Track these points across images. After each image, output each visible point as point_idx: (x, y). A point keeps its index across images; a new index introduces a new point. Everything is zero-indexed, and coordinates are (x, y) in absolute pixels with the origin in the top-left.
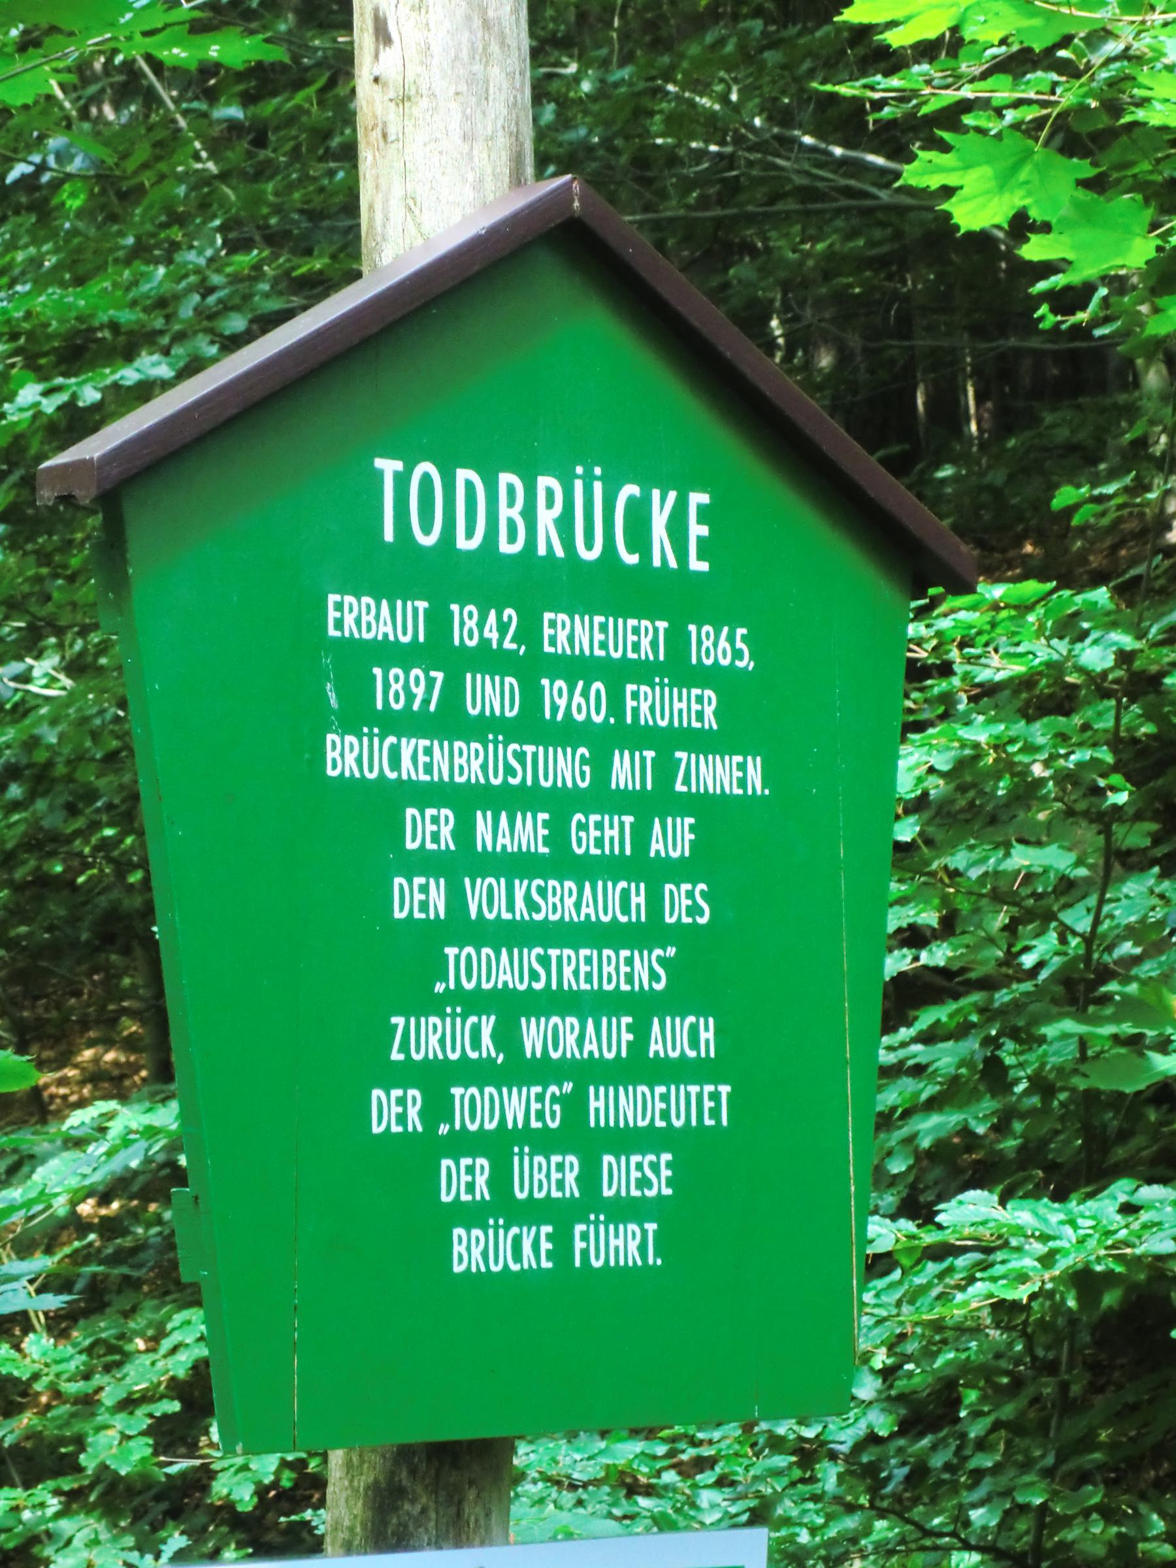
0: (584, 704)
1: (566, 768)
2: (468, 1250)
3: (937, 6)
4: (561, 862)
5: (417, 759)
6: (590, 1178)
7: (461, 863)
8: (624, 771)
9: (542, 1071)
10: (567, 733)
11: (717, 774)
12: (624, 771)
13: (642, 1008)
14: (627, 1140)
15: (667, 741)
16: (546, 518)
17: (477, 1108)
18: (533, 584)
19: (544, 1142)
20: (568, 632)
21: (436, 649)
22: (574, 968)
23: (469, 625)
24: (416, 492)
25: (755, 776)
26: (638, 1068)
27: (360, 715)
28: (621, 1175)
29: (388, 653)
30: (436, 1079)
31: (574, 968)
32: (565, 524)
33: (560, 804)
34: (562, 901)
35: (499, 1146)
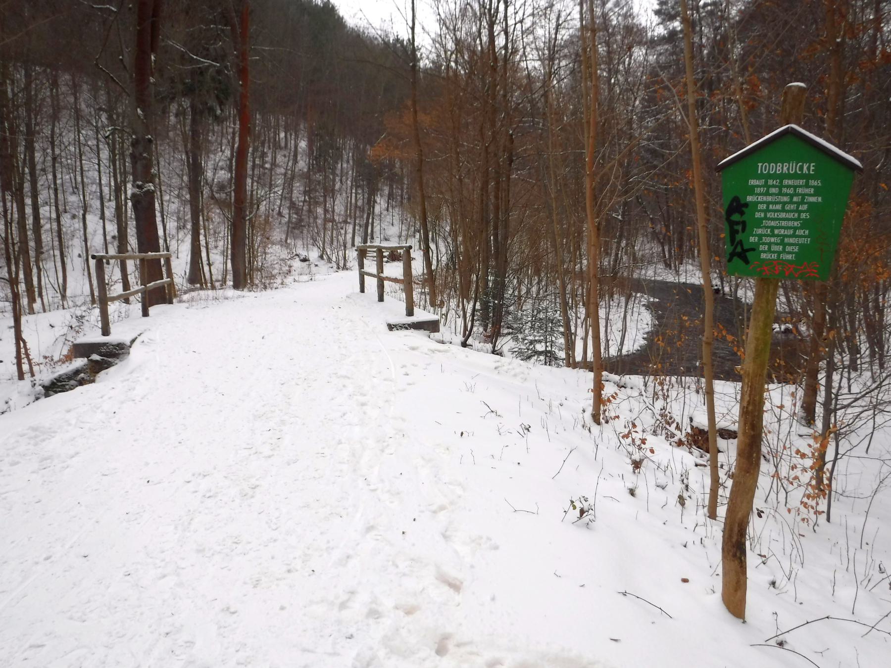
0: (791, 191)
1: (786, 199)
2: (763, 256)
3: (735, 547)
4: (783, 210)
5: (760, 199)
6: (784, 249)
7: (767, 210)
8: (795, 199)
9: (778, 236)
10: (786, 195)
11: (813, 199)
12: (795, 199)
13: (795, 229)
14: (790, 245)
16: (785, 168)
17: (766, 240)
18: (782, 177)
19: (777, 244)
20: (786, 182)
22: (784, 223)
23: (770, 182)
24: (762, 167)
25: (820, 199)
26: (794, 236)
28: (788, 249)
29: (758, 186)
30: (760, 236)
31: (784, 223)
32: (788, 169)
33: (784, 203)
34: (783, 215)
35: (770, 244)
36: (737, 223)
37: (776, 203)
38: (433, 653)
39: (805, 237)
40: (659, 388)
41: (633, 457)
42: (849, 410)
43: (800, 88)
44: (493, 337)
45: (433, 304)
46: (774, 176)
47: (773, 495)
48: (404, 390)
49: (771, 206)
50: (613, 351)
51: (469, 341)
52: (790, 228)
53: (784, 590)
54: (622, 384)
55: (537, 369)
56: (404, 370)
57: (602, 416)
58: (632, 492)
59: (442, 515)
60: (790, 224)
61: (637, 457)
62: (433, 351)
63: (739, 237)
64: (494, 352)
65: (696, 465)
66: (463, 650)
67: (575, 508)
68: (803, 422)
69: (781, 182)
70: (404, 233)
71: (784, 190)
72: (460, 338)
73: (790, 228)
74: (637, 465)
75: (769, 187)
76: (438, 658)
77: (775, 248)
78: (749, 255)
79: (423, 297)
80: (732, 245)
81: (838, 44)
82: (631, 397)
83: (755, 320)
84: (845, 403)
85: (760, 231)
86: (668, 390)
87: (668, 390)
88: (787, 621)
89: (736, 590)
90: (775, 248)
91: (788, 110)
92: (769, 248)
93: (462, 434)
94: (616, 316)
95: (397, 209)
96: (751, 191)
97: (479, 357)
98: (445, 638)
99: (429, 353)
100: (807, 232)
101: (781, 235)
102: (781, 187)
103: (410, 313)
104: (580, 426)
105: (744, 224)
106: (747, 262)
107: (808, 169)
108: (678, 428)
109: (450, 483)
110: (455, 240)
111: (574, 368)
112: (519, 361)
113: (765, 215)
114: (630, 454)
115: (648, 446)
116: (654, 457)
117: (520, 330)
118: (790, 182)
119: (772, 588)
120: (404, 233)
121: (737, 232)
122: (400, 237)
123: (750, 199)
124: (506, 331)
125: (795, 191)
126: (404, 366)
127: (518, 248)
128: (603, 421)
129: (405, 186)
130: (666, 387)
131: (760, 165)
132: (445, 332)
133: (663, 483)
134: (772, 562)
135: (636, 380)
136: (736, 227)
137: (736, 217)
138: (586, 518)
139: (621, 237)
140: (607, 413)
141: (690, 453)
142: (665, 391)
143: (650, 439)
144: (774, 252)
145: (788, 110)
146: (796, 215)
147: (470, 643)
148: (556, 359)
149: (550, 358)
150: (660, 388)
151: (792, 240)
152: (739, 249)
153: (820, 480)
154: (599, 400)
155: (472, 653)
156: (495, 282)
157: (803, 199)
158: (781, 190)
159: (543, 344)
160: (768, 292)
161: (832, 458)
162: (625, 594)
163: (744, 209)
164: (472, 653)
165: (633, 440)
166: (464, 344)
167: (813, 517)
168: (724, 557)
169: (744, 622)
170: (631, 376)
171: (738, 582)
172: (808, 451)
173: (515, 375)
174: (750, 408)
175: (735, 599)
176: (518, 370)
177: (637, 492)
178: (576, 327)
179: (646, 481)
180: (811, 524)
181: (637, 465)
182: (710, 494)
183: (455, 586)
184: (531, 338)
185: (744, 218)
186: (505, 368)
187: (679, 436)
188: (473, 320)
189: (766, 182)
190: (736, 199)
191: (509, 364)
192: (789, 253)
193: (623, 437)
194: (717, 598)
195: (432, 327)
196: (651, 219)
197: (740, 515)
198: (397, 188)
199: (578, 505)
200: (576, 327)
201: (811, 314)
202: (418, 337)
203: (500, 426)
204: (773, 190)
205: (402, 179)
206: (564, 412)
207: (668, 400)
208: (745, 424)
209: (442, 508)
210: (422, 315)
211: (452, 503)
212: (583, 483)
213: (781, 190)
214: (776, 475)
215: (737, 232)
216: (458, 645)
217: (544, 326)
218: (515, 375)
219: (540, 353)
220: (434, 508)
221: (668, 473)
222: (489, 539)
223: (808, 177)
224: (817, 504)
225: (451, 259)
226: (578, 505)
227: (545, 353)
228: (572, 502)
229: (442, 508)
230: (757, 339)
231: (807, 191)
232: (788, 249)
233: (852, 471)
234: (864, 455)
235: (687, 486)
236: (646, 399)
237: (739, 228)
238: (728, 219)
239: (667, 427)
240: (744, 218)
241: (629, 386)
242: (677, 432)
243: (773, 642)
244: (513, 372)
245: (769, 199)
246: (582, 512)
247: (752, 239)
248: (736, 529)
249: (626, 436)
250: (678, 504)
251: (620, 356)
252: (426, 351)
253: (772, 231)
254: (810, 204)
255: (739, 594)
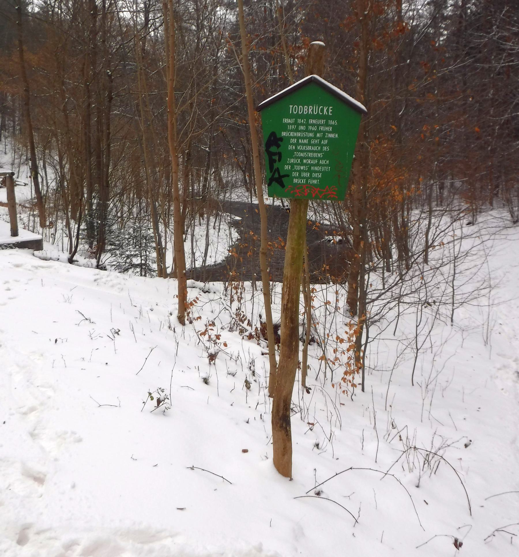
0: (314, 129)
1: (311, 135)
2: (295, 181)
4: (309, 144)
6: (311, 175)
7: (297, 144)
9: (306, 164)
10: (311, 131)
11: (331, 136)
13: (319, 159)
14: (316, 172)
15: (324, 132)
16: (310, 110)
18: (309, 117)
19: (305, 171)
20: (311, 121)
21: (296, 123)
22: (310, 155)
23: (299, 121)
24: (293, 109)
25: (337, 136)
26: (318, 165)
27: (286, 130)
28: (314, 175)
29: (289, 124)
30: (292, 165)
31: (310, 155)
32: (313, 111)
33: (310, 139)
34: (309, 148)
35: (300, 171)
36: (275, 154)
37: (304, 138)
38: (14, 543)
39: (326, 165)
40: (234, 291)
41: (210, 351)
42: (376, 303)
43: (320, 46)
44: (97, 252)
45: (43, 225)
46: (302, 116)
47: (321, 375)
48: (5, 304)
49: (300, 141)
50: (198, 264)
51: (75, 258)
52: (315, 158)
53: (325, 450)
54: (206, 290)
55: (134, 280)
56: (6, 286)
57: (186, 318)
58: (206, 381)
59: (32, 417)
60: (315, 155)
61: (212, 351)
62: (36, 268)
63: (276, 165)
64: (98, 267)
65: (263, 354)
66: (42, 537)
67: (152, 399)
68: (348, 314)
69: (307, 121)
70: (17, 161)
71: (310, 128)
72: (66, 255)
73: (315, 158)
74: (212, 357)
75: (298, 125)
76: (19, 547)
77: (304, 174)
78: (284, 180)
79: (32, 218)
80: (271, 172)
81: (366, 15)
82: (211, 302)
83: (291, 233)
84: (374, 297)
85: (292, 161)
86: (241, 293)
87: (241, 293)
88: (323, 474)
89: (284, 455)
90: (304, 174)
91: (311, 64)
92: (300, 174)
93: (56, 341)
94: (200, 231)
95: (9, 139)
96: (285, 127)
97: (84, 273)
98: (26, 528)
99: (33, 269)
100: (328, 162)
101: (308, 164)
102: (307, 125)
103: (15, 233)
104: (166, 327)
105: (280, 154)
106: (283, 186)
107: (328, 111)
108: (249, 324)
109: (42, 386)
110: (62, 167)
111: (165, 278)
112: (116, 273)
113: (296, 148)
114: (207, 348)
115: (222, 340)
116: (228, 350)
117: (121, 246)
118: (314, 121)
119: (316, 448)
120: (17, 161)
121: (275, 161)
122: (13, 164)
123: (284, 134)
124: (109, 247)
125: (318, 128)
126: (6, 282)
127: (118, 173)
128: (187, 322)
129: (17, 119)
130: (239, 291)
131: (291, 106)
132: (48, 248)
133: (232, 370)
134: (316, 427)
135: (219, 286)
136: (274, 157)
137: (273, 149)
138: (162, 407)
139: (208, 167)
140: (190, 315)
141: (258, 344)
142: (239, 294)
143: (226, 336)
144: (303, 178)
145: (311, 64)
146: (319, 148)
147: (49, 529)
148: (150, 270)
149: (144, 269)
150: (235, 292)
151: (316, 168)
152: (276, 175)
153: (358, 359)
154: (184, 305)
155: (50, 538)
156: (98, 204)
157: (324, 135)
158: (307, 128)
159: (139, 258)
160: (300, 210)
161: (365, 342)
162: (192, 468)
163: (279, 142)
164: (50, 538)
165: (210, 337)
166: (71, 261)
167: (351, 388)
168: (274, 429)
169: (291, 479)
170: (214, 283)
171: (285, 448)
172: (345, 337)
173: (112, 286)
174: (289, 305)
175: (283, 463)
176: (115, 282)
177: (210, 380)
178: (166, 243)
179: (219, 372)
180: (350, 394)
181: (212, 357)
182: (270, 377)
183: (39, 479)
184: (128, 253)
185: (280, 150)
186: (104, 280)
187: (251, 330)
188: (78, 238)
189: (296, 121)
190: (273, 134)
191: (108, 276)
192: (315, 178)
193: (201, 335)
194: (269, 463)
195: (35, 245)
196: (234, 151)
197: (284, 393)
198: (9, 120)
199: (156, 396)
200: (166, 243)
201: (352, 228)
202: (23, 256)
203: (92, 332)
204: (302, 128)
205: (14, 111)
206: (152, 315)
207: (242, 302)
208: (286, 318)
209: (32, 409)
210: (25, 235)
211: (42, 404)
212: (158, 378)
213: (307, 128)
214: (324, 358)
215: (275, 161)
216: (38, 533)
217: (140, 241)
218: (112, 286)
219: (135, 266)
220: (24, 410)
221: (238, 362)
222: (73, 433)
223: (327, 118)
224: (353, 378)
225: (60, 184)
226: (156, 396)
227: (140, 265)
228: (150, 394)
229: (32, 409)
230: (293, 249)
231: (327, 129)
232: (314, 175)
233: (380, 350)
234: (392, 337)
235: (254, 372)
236: (224, 302)
237: (276, 158)
238: (267, 150)
239: (241, 323)
240: (280, 150)
241: (212, 291)
242: (248, 328)
243: (312, 493)
244: (111, 283)
245: (299, 134)
246: (159, 401)
247: (286, 167)
248: (282, 405)
249: (204, 334)
250: (245, 387)
251: (203, 267)
252: (29, 267)
253: (302, 161)
254: (330, 139)
255: (286, 457)
